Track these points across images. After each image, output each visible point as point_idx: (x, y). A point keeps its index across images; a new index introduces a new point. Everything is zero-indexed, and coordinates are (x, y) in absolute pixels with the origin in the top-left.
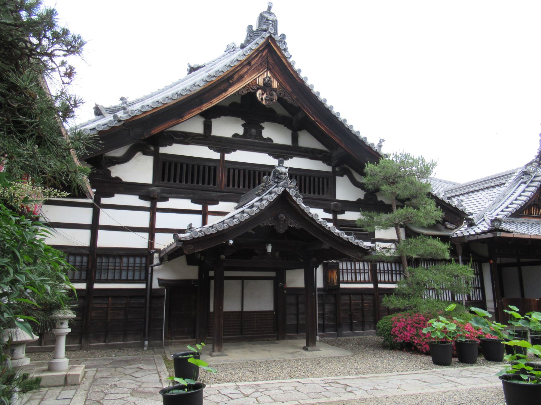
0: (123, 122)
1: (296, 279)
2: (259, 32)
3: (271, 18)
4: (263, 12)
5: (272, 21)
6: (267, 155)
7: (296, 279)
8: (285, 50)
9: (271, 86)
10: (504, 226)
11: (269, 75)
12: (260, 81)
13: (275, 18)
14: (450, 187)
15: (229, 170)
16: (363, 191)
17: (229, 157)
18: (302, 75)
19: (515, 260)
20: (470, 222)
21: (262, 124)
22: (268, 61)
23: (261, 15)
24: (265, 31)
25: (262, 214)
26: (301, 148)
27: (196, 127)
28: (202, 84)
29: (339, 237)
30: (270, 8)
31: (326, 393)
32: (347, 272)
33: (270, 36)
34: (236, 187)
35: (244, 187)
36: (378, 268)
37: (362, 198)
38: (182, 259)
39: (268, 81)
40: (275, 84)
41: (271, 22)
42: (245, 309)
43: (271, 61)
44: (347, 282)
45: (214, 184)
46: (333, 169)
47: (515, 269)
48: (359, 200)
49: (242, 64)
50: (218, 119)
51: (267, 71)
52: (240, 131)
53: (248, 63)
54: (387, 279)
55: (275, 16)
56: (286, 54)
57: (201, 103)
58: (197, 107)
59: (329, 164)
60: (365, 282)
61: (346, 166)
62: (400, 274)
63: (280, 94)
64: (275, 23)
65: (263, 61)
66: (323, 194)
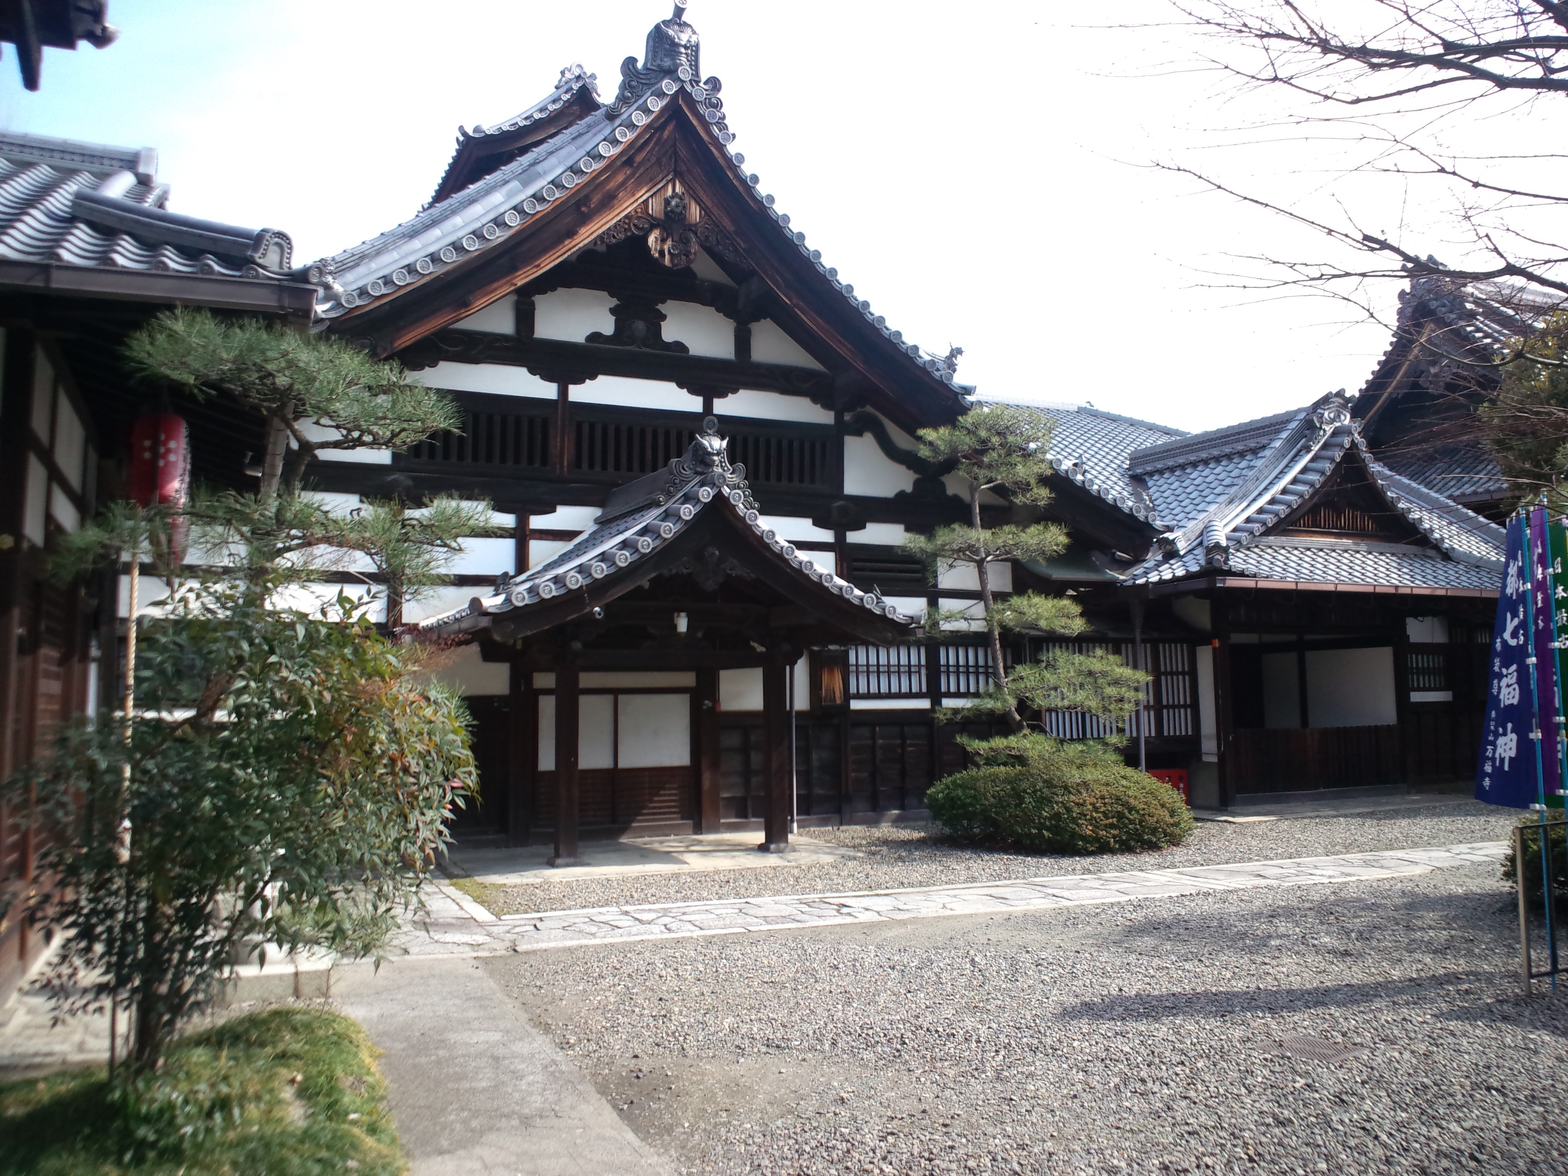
0: (328, 323)
1: (742, 691)
2: (653, 75)
3: (684, 38)
4: (664, 22)
6: (672, 386)
7: (742, 691)
10: (1237, 561)
11: (679, 189)
12: (656, 208)
13: (694, 39)
14: (1149, 442)
15: (579, 425)
16: (911, 473)
17: (579, 393)
18: (762, 189)
19: (1292, 637)
20: (1169, 547)
21: (660, 307)
22: (675, 153)
23: (657, 27)
25: (668, 551)
26: (759, 366)
27: (494, 318)
28: (514, 222)
29: (841, 597)
30: (679, 11)
31: (800, 917)
32: (868, 673)
33: (682, 90)
34: (598, 468)
35: (617, 467)
36: (943, 661)
37: (909, 489)
38: (474, 649)
39: (677, 206)
40: (695, 213)
42: (624, 763)
43: (683, 153)
44: (868, 696)
45: (544, 462)
46: (839, 418)
47: (1292, 658)
48: (901, 495)
50: (550, 294)
52: (607, 326)
54: (963, 689)
55: (694, 32)
57: (513, 269)
58: (502, 277)
59: (826, 406)
60: (910, 695)
61: (869, 409)
62: (987, 675)
66: (813, 481)
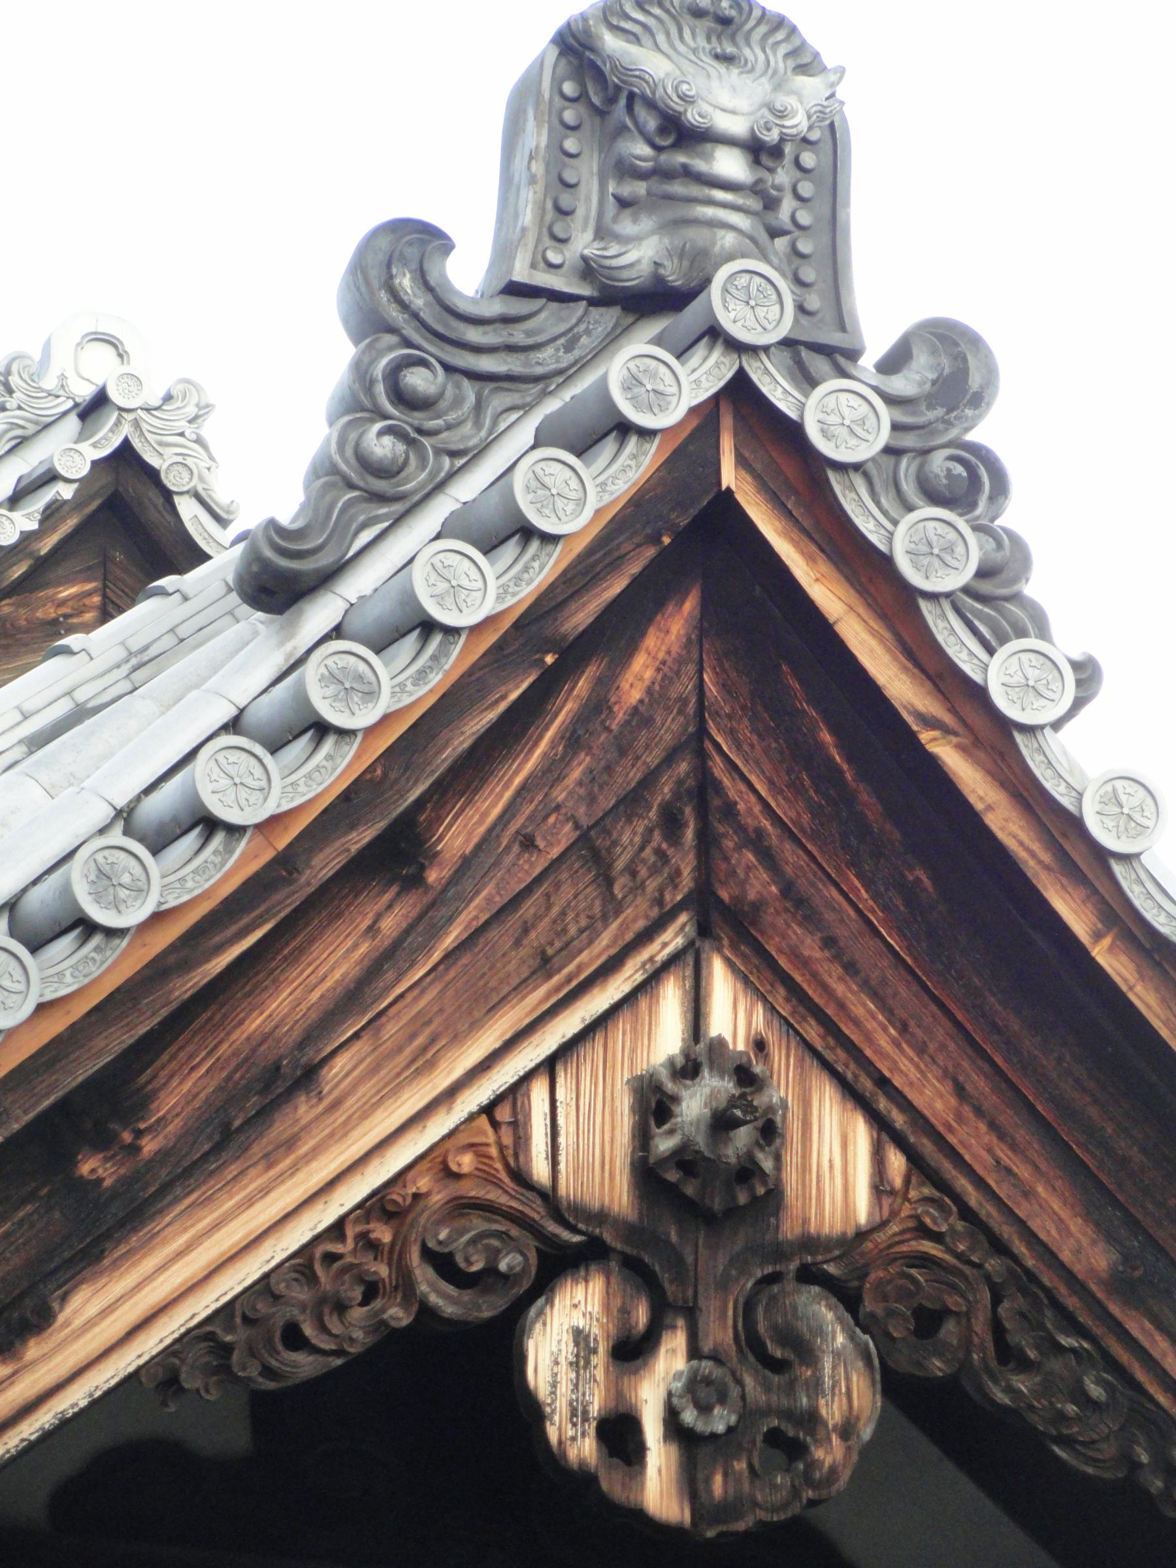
2: (548, 320)
5: (758, 151)
8: (996, 597)
9: (774, 1198)
11: (731, 1014)
12: (583, 1144)
22: (704, 790)
24: (655, 300)
33: (740, 393)
39: (722, 1123)
40: (836, 1169)
41: (729, 164)
43: (753, 784)
49: (285, 865)
51: (689, 961)
53: (378, 840)
55: (806, 62)
56: (1004, 677)
63: (928, 1322)
64: (800, 176)
65: (632, 802)
